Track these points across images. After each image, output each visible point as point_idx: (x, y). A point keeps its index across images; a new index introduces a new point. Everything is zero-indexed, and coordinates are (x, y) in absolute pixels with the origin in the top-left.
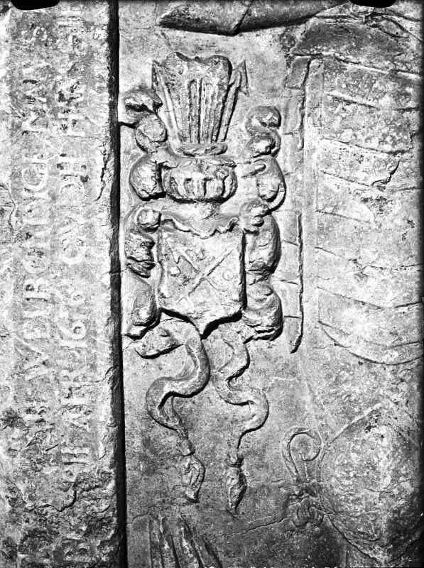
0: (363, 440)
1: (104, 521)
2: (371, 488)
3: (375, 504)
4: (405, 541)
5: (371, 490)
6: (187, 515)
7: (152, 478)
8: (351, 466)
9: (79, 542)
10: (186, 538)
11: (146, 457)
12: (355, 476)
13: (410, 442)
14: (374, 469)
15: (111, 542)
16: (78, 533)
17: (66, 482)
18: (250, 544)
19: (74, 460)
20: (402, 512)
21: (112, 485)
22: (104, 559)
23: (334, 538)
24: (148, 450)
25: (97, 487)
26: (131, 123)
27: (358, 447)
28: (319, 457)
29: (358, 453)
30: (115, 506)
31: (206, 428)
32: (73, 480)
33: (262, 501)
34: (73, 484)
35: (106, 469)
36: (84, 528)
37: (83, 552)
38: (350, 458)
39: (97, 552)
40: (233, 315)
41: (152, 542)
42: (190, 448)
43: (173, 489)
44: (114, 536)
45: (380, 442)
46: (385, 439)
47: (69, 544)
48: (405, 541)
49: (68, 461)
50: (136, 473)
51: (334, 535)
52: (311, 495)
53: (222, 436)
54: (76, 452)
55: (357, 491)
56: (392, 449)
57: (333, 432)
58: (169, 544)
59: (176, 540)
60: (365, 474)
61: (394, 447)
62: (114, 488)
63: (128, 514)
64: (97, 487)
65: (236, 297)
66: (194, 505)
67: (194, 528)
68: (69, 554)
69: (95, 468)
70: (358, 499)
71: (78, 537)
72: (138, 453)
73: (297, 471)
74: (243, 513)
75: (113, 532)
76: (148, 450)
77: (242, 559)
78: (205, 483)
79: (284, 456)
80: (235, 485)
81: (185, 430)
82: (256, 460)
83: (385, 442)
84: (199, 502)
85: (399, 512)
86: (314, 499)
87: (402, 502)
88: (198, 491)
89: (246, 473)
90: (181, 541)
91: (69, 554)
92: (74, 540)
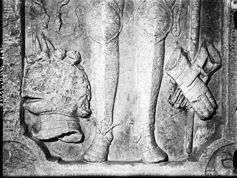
0: (98, 6)
1: (17, 31)
2: (100, 21)
3: (101, 25)
4: (110, 38)
5: (99, 21)
6: (44, 32)
7: (33, 21)
8: (94, 15)
9: (9, 37)
10: (43, 39)
11: (31, 14)
12: (95, 18)
13: (112, 7)
14: (100, 14)
15: (19, 38)
16: (8, 34)
17: (5, 19)
18: (63, 41)
19: (8, 12)
20: (109, 28)
21: (19, 20)
22: (16, 42)
23: (90, 39)
24: (32, 12)
25: (15, 20)
26: (26, 121)
27: (96, 9)
28: (85, 14)
29: (96, 10)
30: (20, 26)
31: (50, 5)
32: (7, 18)
33: (67, 28)
34: (7, 19)
35: (18, 14)
36: (10, 33)
37: (10, 40)
38: (94, 12)
39: (14, 40)
40: (55, 138)
41: (33, 40)
42: (45, 11)
43: (40, 24)
44: (20, 36)
45: (102, 6)
46: (104, 5)
47: (6, 38)
48: (110, 38)
49: (6, 12)
50: (28, 19)
51: (89, 39)
52: (83, 26)
53: (55, 7)
54: (8, 9)
55: (96, 22)
56: (106, 8)
57: (89, 5)
58: (38, 40)
59: (40, 39)
60: (98, 17)
61: (107, 7)
62: (20, 21)
63: (26, 31)
64: (15, 20)
65: (55, 114)
66: (46, 29)
67: (46, 37)
68: (6, 41)
69: (14, 14)
70: (96, 25)
71: (9, 36)
72: (29, 13)
73: (78, 19)
74: (61, 32)
75: (20, 35)
76: (32, 12)
77: (61, 46)
78: (50, 22)
79: (74, 14)
80: (58, 22)
81: (43, 5)
82: (66, 15)
83: (104, 6)
84: (48, 28)
85: (108, 28)
86: (84, 28)
87: (109, 25)
88: (48, 25)
89: (62, 19)
90: (41, 39)
91: (6, 41)
92: (7, 37)
